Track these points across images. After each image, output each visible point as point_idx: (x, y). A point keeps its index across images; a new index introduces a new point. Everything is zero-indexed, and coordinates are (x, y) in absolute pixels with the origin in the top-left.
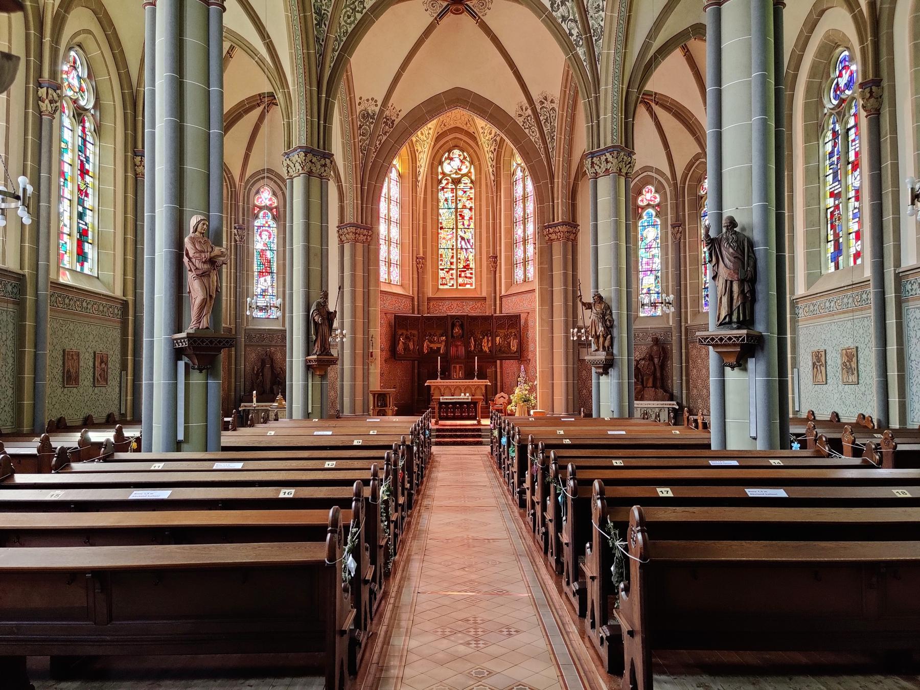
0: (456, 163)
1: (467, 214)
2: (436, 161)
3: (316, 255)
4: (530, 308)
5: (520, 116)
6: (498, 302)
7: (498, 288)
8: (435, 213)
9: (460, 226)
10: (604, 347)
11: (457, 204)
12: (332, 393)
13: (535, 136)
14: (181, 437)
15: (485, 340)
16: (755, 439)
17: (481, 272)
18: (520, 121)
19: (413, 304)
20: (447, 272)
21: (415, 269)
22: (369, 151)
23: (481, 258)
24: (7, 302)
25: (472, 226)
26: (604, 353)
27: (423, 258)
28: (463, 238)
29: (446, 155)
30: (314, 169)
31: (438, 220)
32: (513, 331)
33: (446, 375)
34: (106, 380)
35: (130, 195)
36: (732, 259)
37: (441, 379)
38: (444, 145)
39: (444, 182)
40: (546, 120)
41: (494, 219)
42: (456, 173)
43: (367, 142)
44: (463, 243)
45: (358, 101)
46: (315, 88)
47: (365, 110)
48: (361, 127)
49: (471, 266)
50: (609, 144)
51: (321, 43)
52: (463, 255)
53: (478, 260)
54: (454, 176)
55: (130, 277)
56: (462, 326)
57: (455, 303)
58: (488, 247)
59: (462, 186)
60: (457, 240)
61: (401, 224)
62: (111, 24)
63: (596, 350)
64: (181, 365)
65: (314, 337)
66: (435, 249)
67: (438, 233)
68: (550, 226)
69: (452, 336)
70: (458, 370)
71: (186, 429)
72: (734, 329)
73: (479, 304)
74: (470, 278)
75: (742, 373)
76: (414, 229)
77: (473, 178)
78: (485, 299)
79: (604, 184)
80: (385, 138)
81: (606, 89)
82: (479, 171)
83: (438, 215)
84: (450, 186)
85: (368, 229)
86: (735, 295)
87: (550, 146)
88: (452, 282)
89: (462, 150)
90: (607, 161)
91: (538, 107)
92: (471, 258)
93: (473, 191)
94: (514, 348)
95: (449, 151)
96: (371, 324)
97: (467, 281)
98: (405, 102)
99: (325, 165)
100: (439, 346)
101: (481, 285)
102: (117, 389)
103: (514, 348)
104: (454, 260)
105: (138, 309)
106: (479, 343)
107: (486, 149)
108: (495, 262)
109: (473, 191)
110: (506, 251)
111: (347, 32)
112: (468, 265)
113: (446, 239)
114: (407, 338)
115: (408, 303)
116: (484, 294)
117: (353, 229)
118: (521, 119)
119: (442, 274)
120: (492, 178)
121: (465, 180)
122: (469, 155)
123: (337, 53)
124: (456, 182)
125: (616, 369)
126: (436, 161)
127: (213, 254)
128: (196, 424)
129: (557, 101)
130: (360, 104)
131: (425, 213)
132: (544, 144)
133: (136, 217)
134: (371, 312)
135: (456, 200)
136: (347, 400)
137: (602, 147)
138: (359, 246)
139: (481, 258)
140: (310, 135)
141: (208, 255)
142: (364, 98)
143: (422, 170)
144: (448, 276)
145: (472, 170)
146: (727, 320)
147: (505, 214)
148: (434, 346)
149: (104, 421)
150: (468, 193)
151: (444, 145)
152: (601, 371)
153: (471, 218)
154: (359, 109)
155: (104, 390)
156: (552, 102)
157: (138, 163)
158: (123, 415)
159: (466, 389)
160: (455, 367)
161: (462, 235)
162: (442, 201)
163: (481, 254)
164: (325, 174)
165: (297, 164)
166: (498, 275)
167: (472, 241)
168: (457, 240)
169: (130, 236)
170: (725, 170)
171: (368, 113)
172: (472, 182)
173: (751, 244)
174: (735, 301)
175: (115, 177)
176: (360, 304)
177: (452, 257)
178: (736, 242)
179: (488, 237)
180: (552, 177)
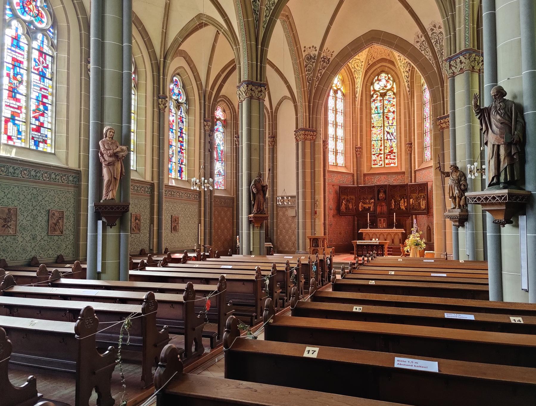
0: (383, 83)
1: (391, 115)
2: (368, 82)
3: (255, 149)
4: (429, 176)
5: (418, 42)
6: (413, 175)
7: (413, 165)
8: (368, 117)
9: (386, 124)
10: (459, 206)
11: (384, 110)
12: (293, 237)
13: (429, 55)
14: (99, 269)
15: (402, 201)
16: (527, 291)
17: (401, 154)
18: (417, 46)
19: (353, 179)
20: (378, 156)
21: (355, 155)
22: (313, 80)
23: (401, 145)
24: (71, 186)
25: (395, 124)
26: (459, 210)
27: (360, 148)
28: (388, 133)
29: (376, 78)
30: (254, 94)
31: (371, 122)
32: (422, 194)
33: (374, 225)
34: (139, 230)
35: (156, 122)
36: (499, 125)
37: (370, 228)
38: (373, 71)
39: (375, 96)
40: (436, 42)
41: (409, 118)
42: (383, 89)
43: (312, 75)
44: (388, 136)
45: (303, 49)
46: (253, 43)
47: (309, 55)
48: (306, 66)
49: (394, 151)
50: (463, 48)
51: (257, 13)
52: (388, 144)
53: (399, 147)
54: (382, 91)
55: (155, 169)
56: (385, 192)
57: (383, 177)
58: (405, 137)
59: (387, 97)
60: (384, 134)
61: (345, 127)
62: (141, 23)
63: (454, 208)
64: (100, 223)
65: (253, 202)
66: (368, 141)
67: (371, 131)
68: (441, 118)
69: (378, 199)
70: (382, 222)
71: (103, 265)
72: (501, 189)
73: (400, 177)
74: (394, 159)
75: (515, 229)
76: (354, 129)
77: (395, 91)
78: (404, 173)
79: (460, 81)
80: (324, 71)
81: (460, 8)
82: (399, 86)
83: (371, 118)
84: (379, 98)
85: (313, 131)
86: (502, 157)
87: (440, 60)
88: (381, 163)
89: (387, 73)
90: (461, 62)
91: (430, 33)
92: (394, 145)
93: (395, 100)
94: (423, 207)
95: (378, 75)
96: (317, 192)
97: (393, 161)
98: (335, 45)
99: (261, 91)
100: (369, 205)
101: (401, 163)
102: (148, 235)
103: (423, 207)
104: (382, 148)
105: (160, 187)
106: (397, 204)
107: (402, 70)
108: (411, 147)
109: (395, 100)
110: (418, 139)
111: (274, 3)
112: (392, 151)
113: (376, 134)
114: (348, 201)
115: (350, 177)
116: (403, 170)
117: (303, 132)
118: (419, 44)
119: (374, 157)
120: (408, 89)
121: (390, 93)
122: (392, 76)
123: (268, 18)
124: (383, 95)
125: (470, 222)
126: (368, 82)
127: (115, 151)
128: (111, 261)
129: (442, 27)
130: (304, 51)
131: (361, 118)
132: (435, 59)
133: (159, 134)
134: (316, 185)
135: (383, 107)
136: (301, 241)
137: (458, 52)
138: (308, 143)
139: (401, 145)
140: (250, 74)
141: (111, 151)
142: (307, 47)
143: (358, 90)
144: (378, 159)
145: (395, 86)
146: (495, 181)
147: (417, 114)
148: (367, 206)
149: (138, 253)
150: (392, 102)
151: (373, 71)
152: (457, 224)
153: (394, 118)
154: (304, 54)
155: (138, 235)
156: (440, 27)
157: (160, 103)
158: (151, 250)
159: (375, 235)
160: (380, 220)
161: (388, 130)
162: (374, 109)
163: (401, 142)
164: (261, 97)
165: (243, 93)
166: (413, 156)
167: (395, 134)
168: (384, 134)
169: (156, 146)
170: (499, 45)
171: (311, 56)
172: (394, 94)
173: (520, 109)
174: (502, 164)
175: (146, 112)
176: (308, 180)
177: (381, 146)
178: (504, 109)
179: (405, 131)
180: (442, 82)
